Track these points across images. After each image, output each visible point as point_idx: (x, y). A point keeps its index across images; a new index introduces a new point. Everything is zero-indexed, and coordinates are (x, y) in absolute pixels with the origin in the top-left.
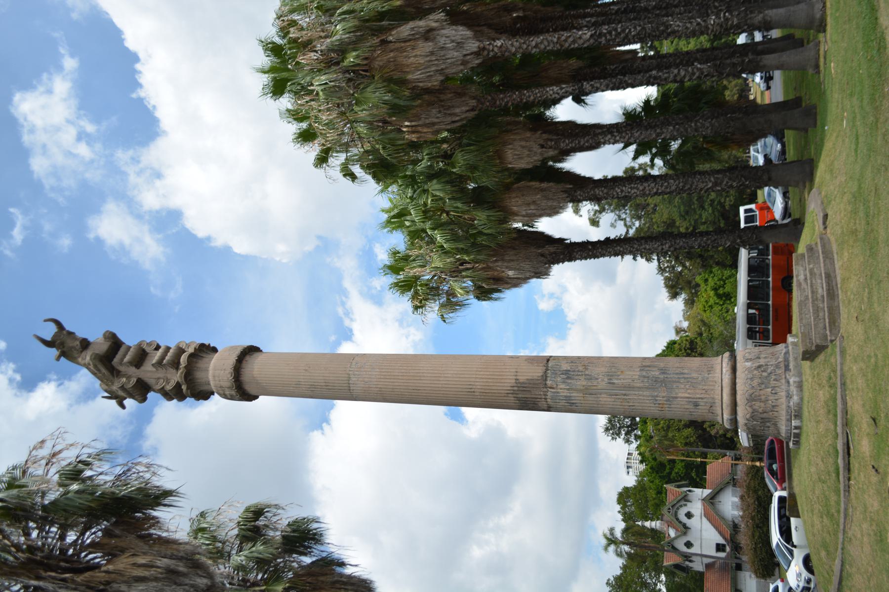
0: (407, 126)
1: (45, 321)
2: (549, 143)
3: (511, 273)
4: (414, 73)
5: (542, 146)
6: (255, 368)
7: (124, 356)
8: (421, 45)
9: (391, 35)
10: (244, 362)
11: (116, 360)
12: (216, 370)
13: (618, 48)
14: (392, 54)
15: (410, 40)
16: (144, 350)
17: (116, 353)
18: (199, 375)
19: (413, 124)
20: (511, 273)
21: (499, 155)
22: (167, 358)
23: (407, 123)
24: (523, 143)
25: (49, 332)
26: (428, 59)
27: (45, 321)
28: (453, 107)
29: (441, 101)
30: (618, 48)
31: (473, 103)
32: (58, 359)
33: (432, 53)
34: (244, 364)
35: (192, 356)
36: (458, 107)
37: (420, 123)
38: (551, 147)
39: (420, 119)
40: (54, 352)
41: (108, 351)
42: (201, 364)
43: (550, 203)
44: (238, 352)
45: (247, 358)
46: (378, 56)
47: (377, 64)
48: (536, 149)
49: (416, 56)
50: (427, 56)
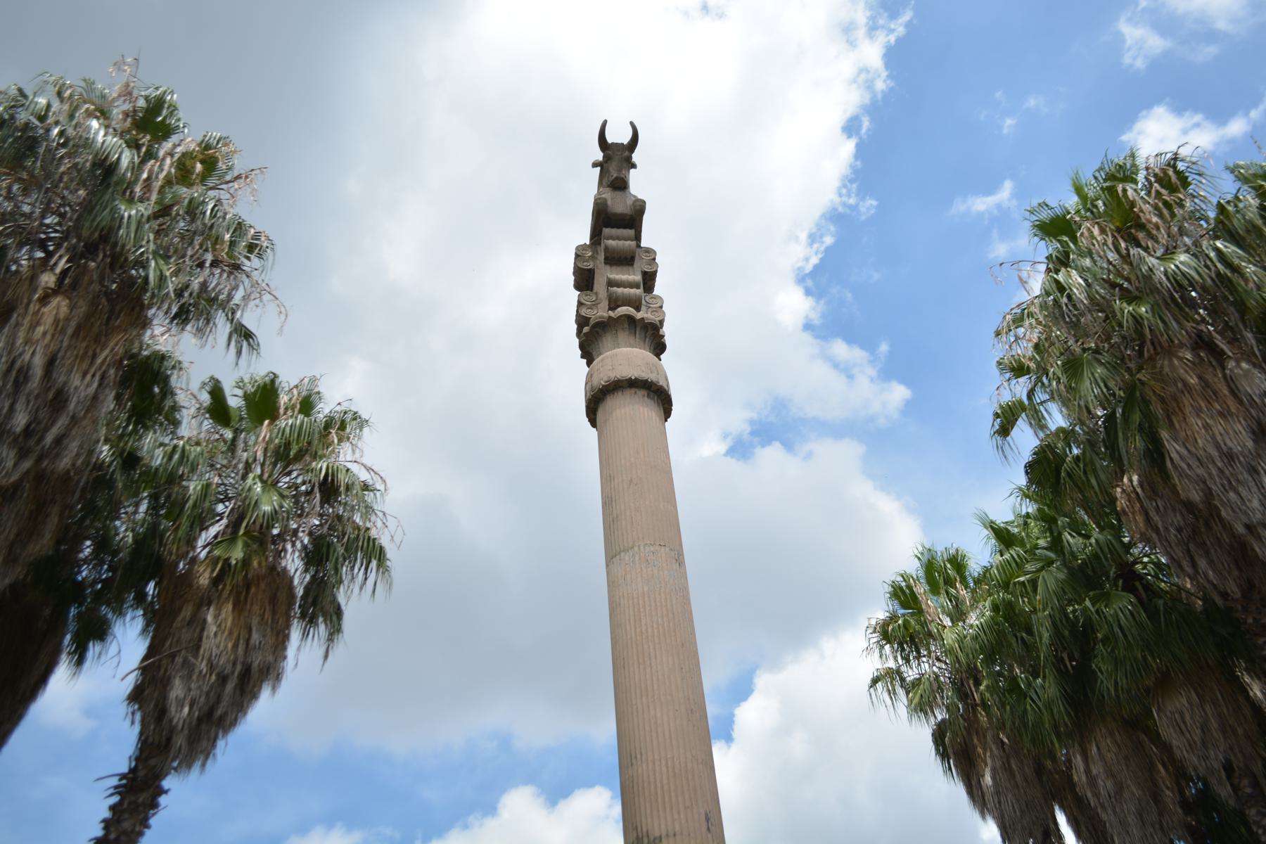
0: (1131, 480)
1: (632, 124)
2: (1245, 782)
3: (988, 779)
4: (1176, 440)
5: (1229, 768)
6: (630, 412)
7: (619, 238)
8: (1238, 427)
9: (1238, 362)
10: (633, 390)
11: (606, 231)
12: (626, 358)
13: (1061, 819)
14: (1193, 380)
15: (1241, 402)
16: (633, 259)
17: (625, 228)
18: (607, 340)
19: (1139, 490)
20: (988, 779)
21: (1164, 683)
22: (620, 290)
23: (1135, 478)
24: (1214, 724)
25: (617, 135)
26: (1215, 453)
27: (632, 124)
28: (1207, 553)
29: (1207, 524)
30: (1061, 819)
31: (1234, 589)
32: (595, 165)
33: (1230, 456)
34: (629, 392)
35: (630, 319)
36: (1211, 562)
37: (1146, 503)
38: (1236, 789)
39: (1150, 499)
40: (599, 156)
41: (615, 215)
42: (623, 336)
43: (1131, 819)
44: (652, 377)
45: (642, 393)
46: (1181, 359)
47: (1163, 364)
48: (1216, 758)
49: (1207, 427)
50: (1218, 446)
